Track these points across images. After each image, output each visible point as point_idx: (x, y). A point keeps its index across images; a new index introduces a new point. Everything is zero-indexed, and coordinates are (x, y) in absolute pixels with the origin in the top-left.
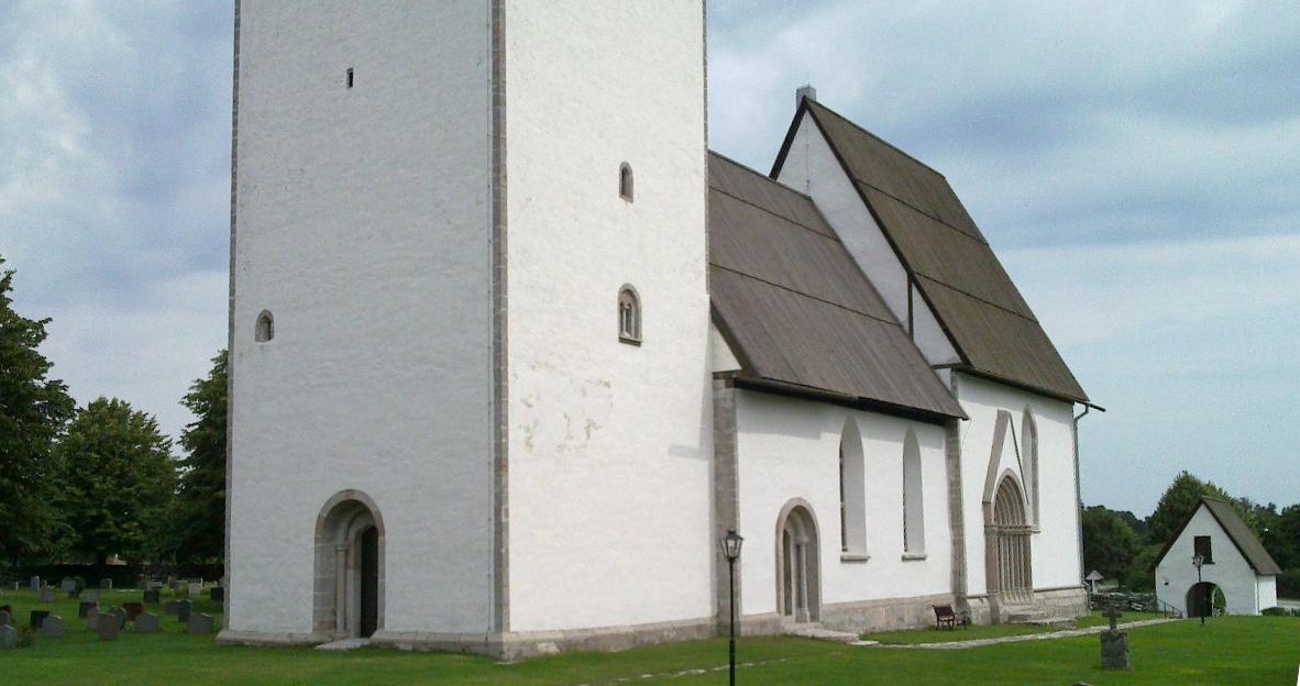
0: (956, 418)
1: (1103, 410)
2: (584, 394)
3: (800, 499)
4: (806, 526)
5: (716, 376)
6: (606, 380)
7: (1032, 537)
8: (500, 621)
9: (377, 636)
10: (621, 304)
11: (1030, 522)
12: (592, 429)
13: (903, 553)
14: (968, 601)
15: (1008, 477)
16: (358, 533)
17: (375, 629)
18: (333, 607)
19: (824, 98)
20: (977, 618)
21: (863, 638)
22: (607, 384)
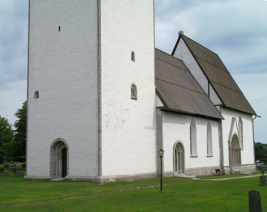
1: (260, 117)
2: (122, 113)
3: (179, 141)
4: (181, 148)
5: (157, 108)
6: (128, 109)
7: (241, 151)
9: (67, 177)
10: (132, 89)
11: (241, 147)
14: (224, 168)
15: (235, 135)
16: (61, 150)
21: (196, 178)
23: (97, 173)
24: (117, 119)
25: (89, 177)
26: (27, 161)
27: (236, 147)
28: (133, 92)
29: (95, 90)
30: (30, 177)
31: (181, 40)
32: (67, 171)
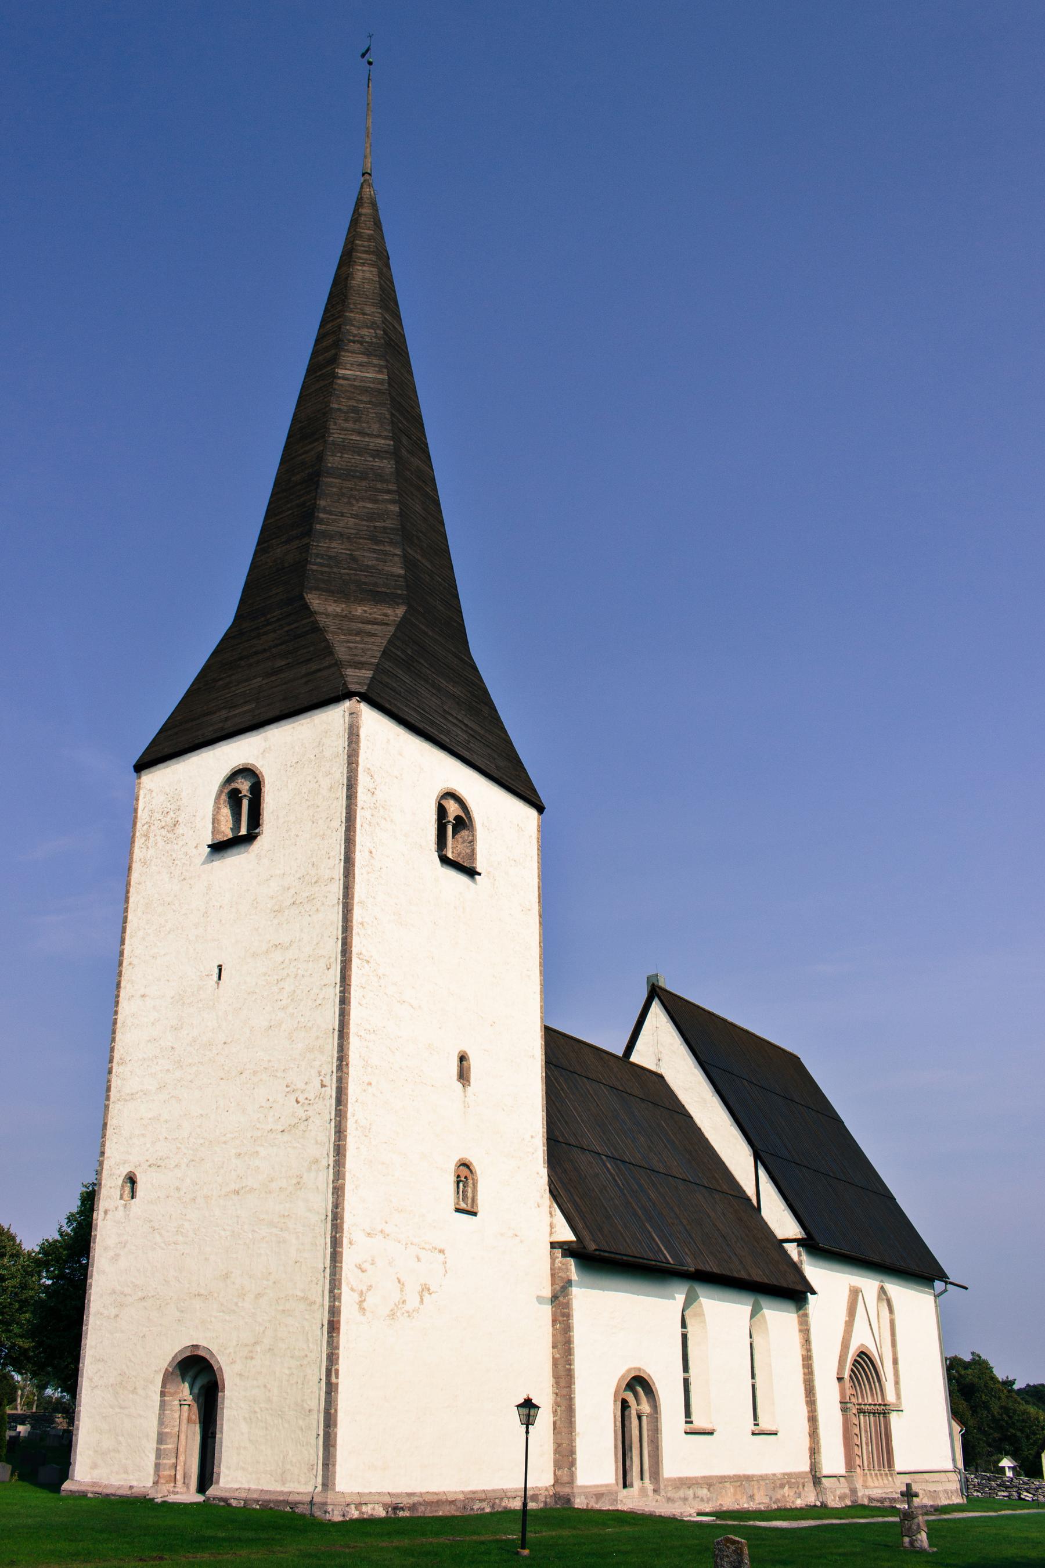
0: (805, 1293)
1: (966, 1288)
2: (419, 1260)
3: (639, 1369)
4: (646, 1394)
5: (553, 1245)
6: (441, 1247)
7: (893, 1417)
8: (328, 1482)
9: (212, 1492)
10: (458, 1176)
11: (891, 1397)
12: (426, 1294)
13: (753, 1428)
14: (824, 1480)
15: (862, 1352)
16: (200, 1389)
17: (211, 1484)
18: (174, 1461)
19: (669, 983)
20: (834, 1500)
21: (699, 1514)
22: (442, 1251)
23: (320, 1479)
24: (399, 1282)
25: (290, 1493)
26: (78, 1425)
27: (873, 1400)
28: (464, 1186)
29: (325, 1178)
30: (83, 1488)
31: (656, 1008)
32: (216, 1469)
